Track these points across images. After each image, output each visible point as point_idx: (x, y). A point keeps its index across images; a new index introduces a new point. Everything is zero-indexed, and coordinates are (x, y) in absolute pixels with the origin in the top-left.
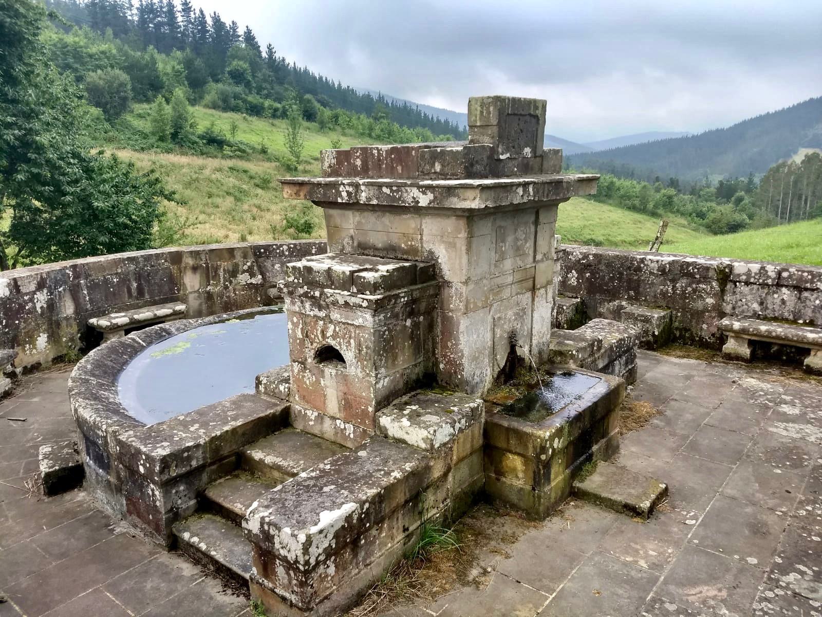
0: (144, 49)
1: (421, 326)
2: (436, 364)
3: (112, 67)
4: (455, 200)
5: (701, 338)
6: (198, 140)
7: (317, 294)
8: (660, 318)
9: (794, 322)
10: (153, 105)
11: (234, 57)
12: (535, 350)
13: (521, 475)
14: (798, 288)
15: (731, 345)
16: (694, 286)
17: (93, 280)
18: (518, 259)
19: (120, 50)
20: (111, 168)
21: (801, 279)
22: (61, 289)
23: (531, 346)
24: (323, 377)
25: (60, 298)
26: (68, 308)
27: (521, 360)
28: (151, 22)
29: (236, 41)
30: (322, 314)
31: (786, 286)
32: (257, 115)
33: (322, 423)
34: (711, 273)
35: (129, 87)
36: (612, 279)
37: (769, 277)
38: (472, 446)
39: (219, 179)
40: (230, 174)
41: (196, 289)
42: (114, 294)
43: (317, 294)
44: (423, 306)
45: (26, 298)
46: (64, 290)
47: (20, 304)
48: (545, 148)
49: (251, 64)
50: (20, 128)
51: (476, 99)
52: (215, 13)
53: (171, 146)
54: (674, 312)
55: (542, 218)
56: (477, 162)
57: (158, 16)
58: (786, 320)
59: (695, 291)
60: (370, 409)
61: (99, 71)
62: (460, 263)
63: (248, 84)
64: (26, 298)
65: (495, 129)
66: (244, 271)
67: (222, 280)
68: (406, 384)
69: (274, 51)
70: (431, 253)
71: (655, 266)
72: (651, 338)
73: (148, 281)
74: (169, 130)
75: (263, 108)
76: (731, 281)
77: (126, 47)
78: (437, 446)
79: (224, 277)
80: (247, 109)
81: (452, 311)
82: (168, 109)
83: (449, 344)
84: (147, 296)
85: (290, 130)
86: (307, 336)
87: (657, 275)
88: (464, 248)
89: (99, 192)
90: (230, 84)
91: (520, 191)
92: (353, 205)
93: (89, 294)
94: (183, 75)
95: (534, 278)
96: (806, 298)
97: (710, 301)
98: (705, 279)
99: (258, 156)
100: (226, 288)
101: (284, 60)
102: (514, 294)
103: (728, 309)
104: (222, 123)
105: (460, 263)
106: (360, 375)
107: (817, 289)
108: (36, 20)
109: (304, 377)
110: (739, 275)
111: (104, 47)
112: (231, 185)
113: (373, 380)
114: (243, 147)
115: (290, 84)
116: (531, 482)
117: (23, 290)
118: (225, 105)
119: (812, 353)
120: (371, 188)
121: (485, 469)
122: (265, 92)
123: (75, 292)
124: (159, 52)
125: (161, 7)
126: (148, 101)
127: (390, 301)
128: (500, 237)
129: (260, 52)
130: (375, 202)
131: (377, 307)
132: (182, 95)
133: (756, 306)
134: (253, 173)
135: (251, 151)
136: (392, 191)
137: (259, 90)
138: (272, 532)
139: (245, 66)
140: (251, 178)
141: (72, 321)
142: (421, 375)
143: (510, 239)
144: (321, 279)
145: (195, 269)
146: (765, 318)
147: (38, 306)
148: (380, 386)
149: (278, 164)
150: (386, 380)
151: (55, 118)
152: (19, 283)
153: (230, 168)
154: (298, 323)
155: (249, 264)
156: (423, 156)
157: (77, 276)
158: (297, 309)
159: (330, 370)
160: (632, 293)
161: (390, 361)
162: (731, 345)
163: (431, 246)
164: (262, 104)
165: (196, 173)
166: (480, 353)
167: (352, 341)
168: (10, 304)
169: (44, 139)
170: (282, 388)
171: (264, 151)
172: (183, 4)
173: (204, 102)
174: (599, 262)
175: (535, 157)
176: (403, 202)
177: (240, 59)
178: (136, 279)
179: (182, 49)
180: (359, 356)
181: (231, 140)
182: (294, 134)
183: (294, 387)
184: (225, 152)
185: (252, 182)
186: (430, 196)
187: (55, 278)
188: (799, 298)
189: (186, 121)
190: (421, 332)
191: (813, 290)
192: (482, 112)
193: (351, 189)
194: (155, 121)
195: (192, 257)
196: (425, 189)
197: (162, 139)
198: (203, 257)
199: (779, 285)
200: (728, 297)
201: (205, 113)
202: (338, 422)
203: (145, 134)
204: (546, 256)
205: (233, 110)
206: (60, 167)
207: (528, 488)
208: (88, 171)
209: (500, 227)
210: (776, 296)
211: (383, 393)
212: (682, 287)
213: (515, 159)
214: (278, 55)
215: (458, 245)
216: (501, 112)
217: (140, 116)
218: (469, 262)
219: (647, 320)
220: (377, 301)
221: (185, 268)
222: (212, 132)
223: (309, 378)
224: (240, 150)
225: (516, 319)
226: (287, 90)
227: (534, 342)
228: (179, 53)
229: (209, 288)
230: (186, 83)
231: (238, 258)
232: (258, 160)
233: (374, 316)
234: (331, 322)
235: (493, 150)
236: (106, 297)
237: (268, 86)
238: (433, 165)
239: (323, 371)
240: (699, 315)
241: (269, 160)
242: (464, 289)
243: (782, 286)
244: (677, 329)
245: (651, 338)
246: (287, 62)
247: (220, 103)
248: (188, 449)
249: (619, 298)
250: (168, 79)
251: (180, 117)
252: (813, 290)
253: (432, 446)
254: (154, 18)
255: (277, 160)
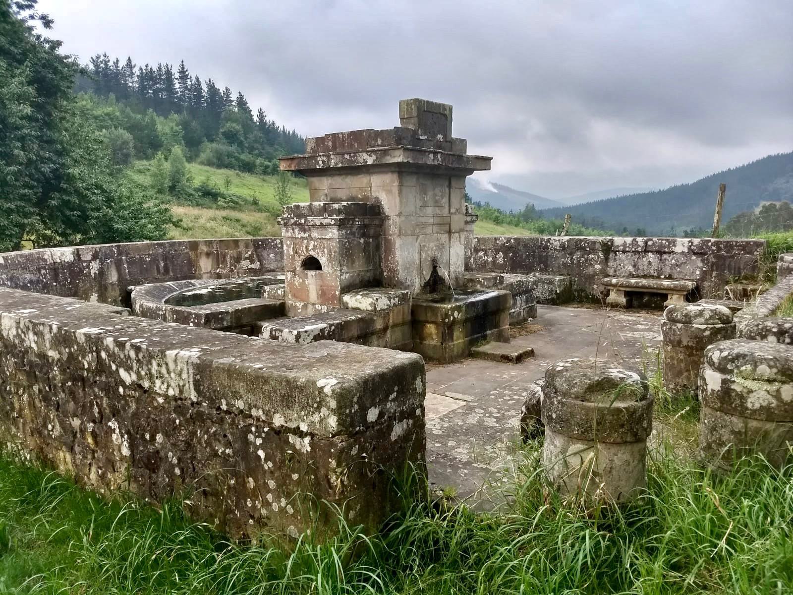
0: (144, 113)
1: (371, 245)
2: (382, 273)
3: (116, 128)
4: (388, 158)
5: (593, 296)
6: (193, 193)
7: (303, 221)
8: (560, 281)
9: (658, 277)
10: (154, 162)
11: (228, 119)
12: (453, 276)
13: (434, 337)
14: (660, 252)
15: (613, 297)
16: (586, 256)
17: (131, 258)
18: (437, 208)
19: (123, 112)
20: (128, 198)
21: (661, 245)
22: (109, 261)
23: (449, 272)
24: (307, 278)
25: (108, 268)
26: (113, 277)
27: (442, 280)
28: (150, 88)
29: (229, 106)
30: (306, 235)
31: (651, 252)
32: (249, 172)
33: (306, 309)
34: (597, 246)
35: (131, 145)
36: (528, 256)
37: (639, 246)
38: (403, 318)
39: (214, 227)
40: (223, 222)
41: (209, 270)
42: (146, 269)
43: (303, 221)
44: (372, 232)
45: (84, 264)
46: (111, 262)
47: (80, 268)
48: (453, 136)
49: (243, 126)
50: (54, 163)
51: (404, 101)
52: (210, 80)
53: (168, 198)
54: (573, 278)
55: (453, 183)
56: (404, 138)
57: (158, 83)
58: (652, 277)
59: (587, 260)
60: (337, 293)
61: (104, 131)
62: (395, 202)
63: (241, 144)
64: (84, 264)
65: (416, 119)
66: (246, 258)
67: (229, 264)
68: (361, 281)
69: (264, 114)
70: (377, 198)
71: (557, 243)
72: (554, 296)
73: (173, 262)
74: (167, 183)
75: (255, 166)
76: (613, 251)
77: (128, 110)
78: (378, 309)
79: (230, 263)
80: (239, 166)
81: (391, 235)
82: (167, 166)
83: (390, 258)
84: (171, 274)
85: (280, 184)
86: (296, 252)
87: (559, 251)
88: (397, 192)
89: (119, 216)
90: (224, 143)
91: (432, 156)
92: (326, 172)
93: (128, 268)
94: (181, 135)
95: (450, 224)
96: (665, 259)
97: (598, 267)
98: (593, 251)
99: (250, 207)
100: (232, 271)
101: (274, 124)
102: (435, 232)
103: (611, 272)
104: (217, 178)
105: (395, 202)
106: (331, 271)
107: (673, 252)
108: (70, 76)
109: (294, 280)
110: (618, 246)
111: (109, 109)
112: (224, 232)
113: (338, 273)
114: (236, 199)
115: (280, 145)
116: (440, 340)
117: (83, 258)
118: (220, 162)
119: (669, 297)
120: (337, 156)
121: (413, 338)
122: (257, 152)
123: (118, 265)
124: (158, 115)
125: (160, 75)
126: (147, 158)
127: (349, 221)
128: (423, 192)
129: (252, 116)
130: (340, 165)
131: (341, 225)
132: (180, 152)
133: (631, 268)
134: (245, 222)
135: (243, 203)
136: (350, 157)
137: (251, 150)
138: (277, 335)
139: (238, 127)
140: (243, 226)
141: (116, 286)
142: (371, 278)
143: (430, 193)
144: (305, 212)
145: (208, 255)
146: (638, 277)
147: (92, 272)
148: (343, 277)
149: (268, 214)
150: (348, 275)
151: (82, 157)
152: (80, 253)
153: (224, 218)
154: (291, 244)
155: (250, 253)
156: (370, 135)
157: (120, 253)
158: (290, 235)
159: (311, 273)
160: (542, 266)
161: (350, 264)
162: (613, 297)
163: (377, 194)
164: (254, 162)
165: (191, 221)
166: (411, 265)
167: (325, 250)
168: (74, 268)
169: (75, 171)
170: (279, 292)
171: (255, 203)
172: (180, 73)
173: (199, 160)
174: (519, 244)
175: (446, 142)
176: (358, 163)
177: (233, 122)
178: (163, 260)
179: (179, 111)
180: (330, 260)
181: (225, 192)
182: (283, 187)
183: (288, 289)
184: (219, 203)
185: (244, 229)
186: (374, 157)
187: (105, 252)
188: (661, 260)
189: (183, 175)
190: (371, 249)
191: (670, 253)
192: (407, 109)
193: (324, 159)
194: (155, 175)
195: (206, 245)
196: (370, 153)
197: (160, 191)
198: (215, 246)
199: (646, 251)
200: (611, 264)
201: (200, 170)
202: (317, 306)
203: (145, 187)
204: (458, 211)
205: (227, 167)
206: (86, 196)
207: (439, 344)
208: (109, 200)
209: (422, 184)
210: (644, 259)
211: (345, 283)
212: (577, 258)
213: (431, 140)
214: (269, 119)
215: (393, 191)
216: (419, 109)
217: (140, 172)
218: (401, 201)
219: (551, 283)
220: (340, 219)
221: (201, 253)
222: (207, 186)
223: (298, 281)
224: (233, 201)
225: (436, 250)
226: (276, 150)
227: (452, 270)
228: (176, 116)
229: (218, 270)
230: (183, 142)
231: (242, 248)
232: (250, 210)
233: (339, 230)
234: (312, 239)
235: (415, 132)
236: (141, 271)
237: (260, 147)
238: (377, 141)
239: (307, 274)
240: (590, 278)
241: (260, 210)
242: (397, 219)
243: (649, 252)
244: (576, 290)
245: (554, 296)
246: (276, 125)
247: (215, 160)
248: (222, 313)
249: (533, 271)
250: (167, 139)
251: (178, 172)
252: (670, 253)
253: (375, 308)
254: (153, 85)
255: (268, 210)
